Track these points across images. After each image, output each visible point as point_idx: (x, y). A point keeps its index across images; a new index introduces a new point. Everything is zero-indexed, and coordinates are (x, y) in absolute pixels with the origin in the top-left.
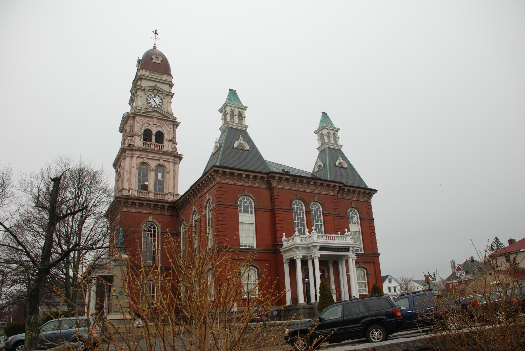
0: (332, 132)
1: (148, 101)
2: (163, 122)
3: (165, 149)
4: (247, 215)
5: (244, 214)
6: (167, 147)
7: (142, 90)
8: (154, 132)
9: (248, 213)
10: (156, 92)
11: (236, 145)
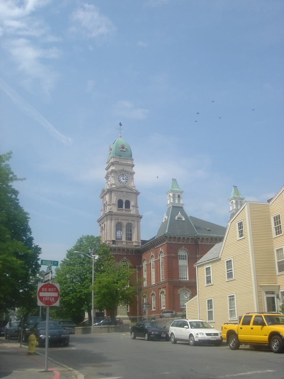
0: (239, 201)
1: (119, 180)
2: (129, 194)
3: (132, 213)
4: (183, 261)
5: (181, 260)
6: (133, 211)
7: (115, 172)
8: (124, 202)
9: (184, 259)
10: (123, 172)
11: (176, 218)
